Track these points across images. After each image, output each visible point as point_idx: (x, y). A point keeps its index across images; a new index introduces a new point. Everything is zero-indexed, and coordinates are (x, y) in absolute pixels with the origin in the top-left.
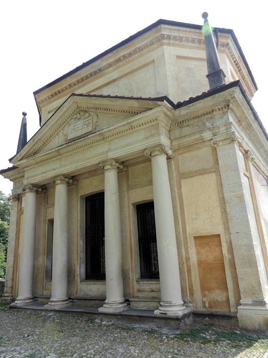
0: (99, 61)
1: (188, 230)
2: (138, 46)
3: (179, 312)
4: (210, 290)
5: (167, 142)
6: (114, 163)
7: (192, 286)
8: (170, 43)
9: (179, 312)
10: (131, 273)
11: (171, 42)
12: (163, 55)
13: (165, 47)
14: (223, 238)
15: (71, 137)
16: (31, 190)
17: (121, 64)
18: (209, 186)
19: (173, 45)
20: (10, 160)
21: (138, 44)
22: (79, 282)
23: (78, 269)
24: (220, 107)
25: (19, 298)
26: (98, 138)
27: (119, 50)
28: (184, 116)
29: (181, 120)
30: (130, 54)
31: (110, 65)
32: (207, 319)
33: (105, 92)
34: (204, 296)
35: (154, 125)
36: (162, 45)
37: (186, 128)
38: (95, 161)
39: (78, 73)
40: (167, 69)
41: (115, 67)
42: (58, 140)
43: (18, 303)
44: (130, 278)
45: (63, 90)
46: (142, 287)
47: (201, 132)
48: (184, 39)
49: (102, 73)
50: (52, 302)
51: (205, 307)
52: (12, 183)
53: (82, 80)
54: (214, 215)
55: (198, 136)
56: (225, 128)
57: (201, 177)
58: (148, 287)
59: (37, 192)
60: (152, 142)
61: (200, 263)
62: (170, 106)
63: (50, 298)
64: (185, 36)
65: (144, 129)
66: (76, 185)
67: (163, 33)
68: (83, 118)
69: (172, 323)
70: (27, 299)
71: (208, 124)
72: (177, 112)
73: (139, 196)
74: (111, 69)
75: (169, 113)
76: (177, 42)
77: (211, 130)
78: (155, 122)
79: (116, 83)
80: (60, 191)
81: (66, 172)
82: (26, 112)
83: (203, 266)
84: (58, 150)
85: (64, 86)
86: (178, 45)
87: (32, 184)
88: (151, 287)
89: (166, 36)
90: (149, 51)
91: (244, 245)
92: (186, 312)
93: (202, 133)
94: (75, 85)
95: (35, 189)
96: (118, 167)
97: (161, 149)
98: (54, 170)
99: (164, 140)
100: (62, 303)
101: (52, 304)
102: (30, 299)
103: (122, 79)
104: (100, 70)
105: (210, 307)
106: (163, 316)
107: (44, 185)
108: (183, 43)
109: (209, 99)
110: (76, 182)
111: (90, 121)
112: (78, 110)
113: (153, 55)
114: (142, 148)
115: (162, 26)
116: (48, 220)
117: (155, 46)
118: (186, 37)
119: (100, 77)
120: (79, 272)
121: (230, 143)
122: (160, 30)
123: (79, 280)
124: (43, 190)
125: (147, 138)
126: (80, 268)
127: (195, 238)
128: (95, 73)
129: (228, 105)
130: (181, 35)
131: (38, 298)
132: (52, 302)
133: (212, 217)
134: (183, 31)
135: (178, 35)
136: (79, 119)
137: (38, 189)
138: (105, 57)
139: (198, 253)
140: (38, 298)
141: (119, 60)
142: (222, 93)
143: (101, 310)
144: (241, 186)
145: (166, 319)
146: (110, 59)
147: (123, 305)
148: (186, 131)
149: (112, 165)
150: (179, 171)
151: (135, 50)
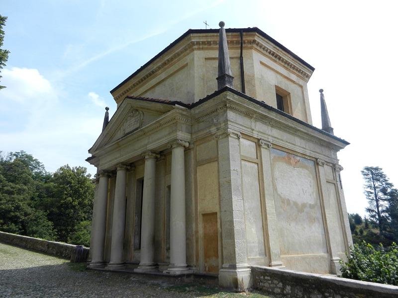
0: (151, 65)
1: (199, 208)
2: (176, 52)
3: (177, 272)
5: (186, 136)
6: (150, 154)
7: (198, 253)
8: (200, 48)
9: (177, 272)
10: (163, 243)
11: (201, 47)
12: (193, 59)
13: (195, 52)
15: (127, 131)
17: (166, 66)
18: (213, 172)
19: (202, 49)
20: (89, 151)
21: (177, 49)
23: (133, 240)
24: (221, 107)
25: (111, 263)
26: (141, 133)
27: (164, 55)
29: (197, 117)
30: (172, 58)
31: (159, 68)
33: (149, 95)
35: (174, 124)
36: (193, 50)
37: (201, 123)
38: (139, 152)
39: (138, 75)
41: (162, 69)
42: (120, 134)
43: (91, 265)
44: (161, 247)
45: (130, 89)
47: (210, 127)
48: (212, 43)
49: (155, 74)
50: (110, 264)
51: (205, 270)
53: (142, 80)
56: (224, 124)
57: (209, 165)
59: (127, 170)
60: (172, 137)
61: (205, 235)
62: (183, 107)
63: (140, 262)
64: (212, 40)
65: (169, 125)
66: (164, 159)
67: (193, 40)
68: (135, 115)
69: (172, 279)
70: (97, 263)
71: (215, 121)
72: (192, 111)
74: (160, 71)
75: (184, 113)
76: (206, 46)
77: (216, 126)
78: (175, 121)
79: (163, 83)
80: (120, 175)
81: (106, 168)
82: (108, 107)
84: (118, 143)
85: (130, 86)
86: (207, 49)
87: (104, 170)
89: (195, 43)
90: (185, 56)
91: (228, 221)
92: (186, 272)
94: (137, 84)
95: (106, 174)
96: (126, 168)
97: (175, 143)
98: (116, 158)
99: (182, 135)
100: (116, 266)
101: (110, 266)
102: (101, 263)
103: (168, 80)
104: (153, 72)
105: (209, 271)
106: (168, 274)
108: (212, 46)
109: (211, 100)
110: (133, 168)
112: (132, 109)
113: (188, 59)
114: (166, 141)
117: (188, 51)
118: (214, 41)
119: (154, 77)
120: (133, 243)
121: (226, 137)
123: (133, 249)
124: (132, 166)
125: (169, 134)
126: (134, 240)
127: (204, 215)
128: (150, 74)
129: (226, 105)
130: (209, 40)
131: (105, 262)
132: (110, 264)
134: (211, 36)
135: (205, 40)
136: (133, 116)
137: (127, 167)
138: (155, 61)
139: (205, 227)
140: (105, 262)
141: (165, 64)
142: (219, 96)
143: (136, 270)
144: (230, 173)
145: (169, 277)
146: (159, 63)
147: (150, 267)
148: (202, 125)
149: (149, 155)
150: (196, 160)
151: (175, 55)
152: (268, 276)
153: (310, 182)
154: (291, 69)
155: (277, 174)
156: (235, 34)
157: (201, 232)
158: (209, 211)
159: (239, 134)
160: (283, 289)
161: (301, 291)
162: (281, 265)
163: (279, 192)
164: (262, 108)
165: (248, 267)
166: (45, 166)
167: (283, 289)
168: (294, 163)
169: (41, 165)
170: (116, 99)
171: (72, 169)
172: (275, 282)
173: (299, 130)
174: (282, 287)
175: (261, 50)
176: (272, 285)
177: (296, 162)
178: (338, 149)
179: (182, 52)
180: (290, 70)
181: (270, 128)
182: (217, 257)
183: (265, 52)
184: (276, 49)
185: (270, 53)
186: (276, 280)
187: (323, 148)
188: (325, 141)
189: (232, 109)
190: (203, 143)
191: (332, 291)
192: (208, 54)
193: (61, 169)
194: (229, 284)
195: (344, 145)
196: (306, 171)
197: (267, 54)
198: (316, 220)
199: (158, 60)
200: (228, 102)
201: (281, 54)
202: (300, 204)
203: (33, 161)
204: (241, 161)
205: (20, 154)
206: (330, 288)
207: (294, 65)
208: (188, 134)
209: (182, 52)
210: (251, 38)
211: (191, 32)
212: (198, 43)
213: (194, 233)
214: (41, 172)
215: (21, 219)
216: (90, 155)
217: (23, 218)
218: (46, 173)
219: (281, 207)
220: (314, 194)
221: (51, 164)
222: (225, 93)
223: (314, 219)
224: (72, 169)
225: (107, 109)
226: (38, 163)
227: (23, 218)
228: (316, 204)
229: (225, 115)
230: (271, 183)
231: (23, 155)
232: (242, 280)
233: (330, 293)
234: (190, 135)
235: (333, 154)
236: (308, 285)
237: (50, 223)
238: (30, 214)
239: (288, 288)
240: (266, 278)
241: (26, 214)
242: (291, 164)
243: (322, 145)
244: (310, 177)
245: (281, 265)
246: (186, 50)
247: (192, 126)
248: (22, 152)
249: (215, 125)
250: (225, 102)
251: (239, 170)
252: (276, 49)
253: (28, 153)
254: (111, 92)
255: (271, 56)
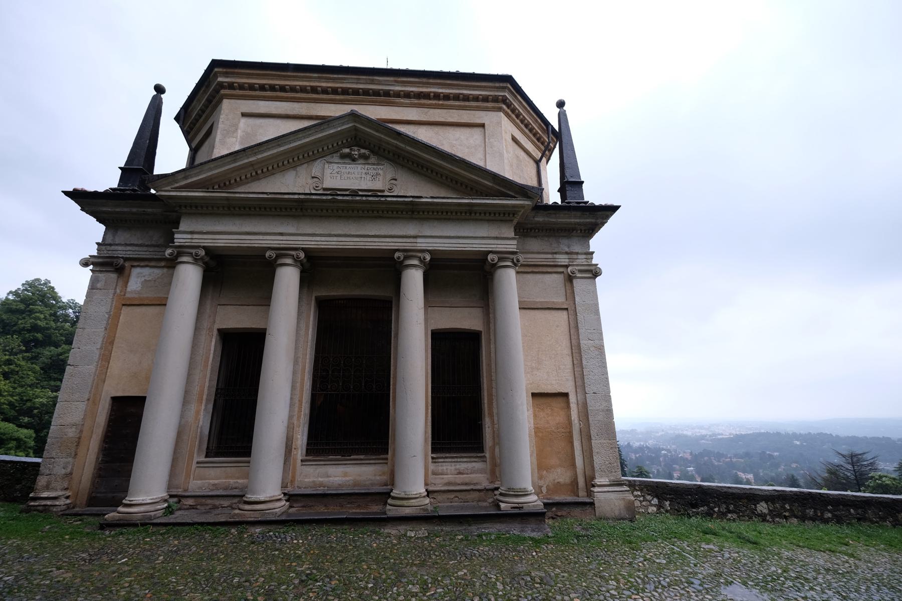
4: (548, 469)
14: (572, 398)
16: (196, 260)
18: (557, 326)
22: (299, 462)
28: (538, 222)
32: (554, 509)
46: (440, 468)
52: (102, 228)
54: (562, 367)
58: (453, 468)
73: (238, 318)
83: (540, 435)
88: (458, 467)
106: (516, 511)
116: (219, 330)
127: (534, 395)
133: (560, 369)
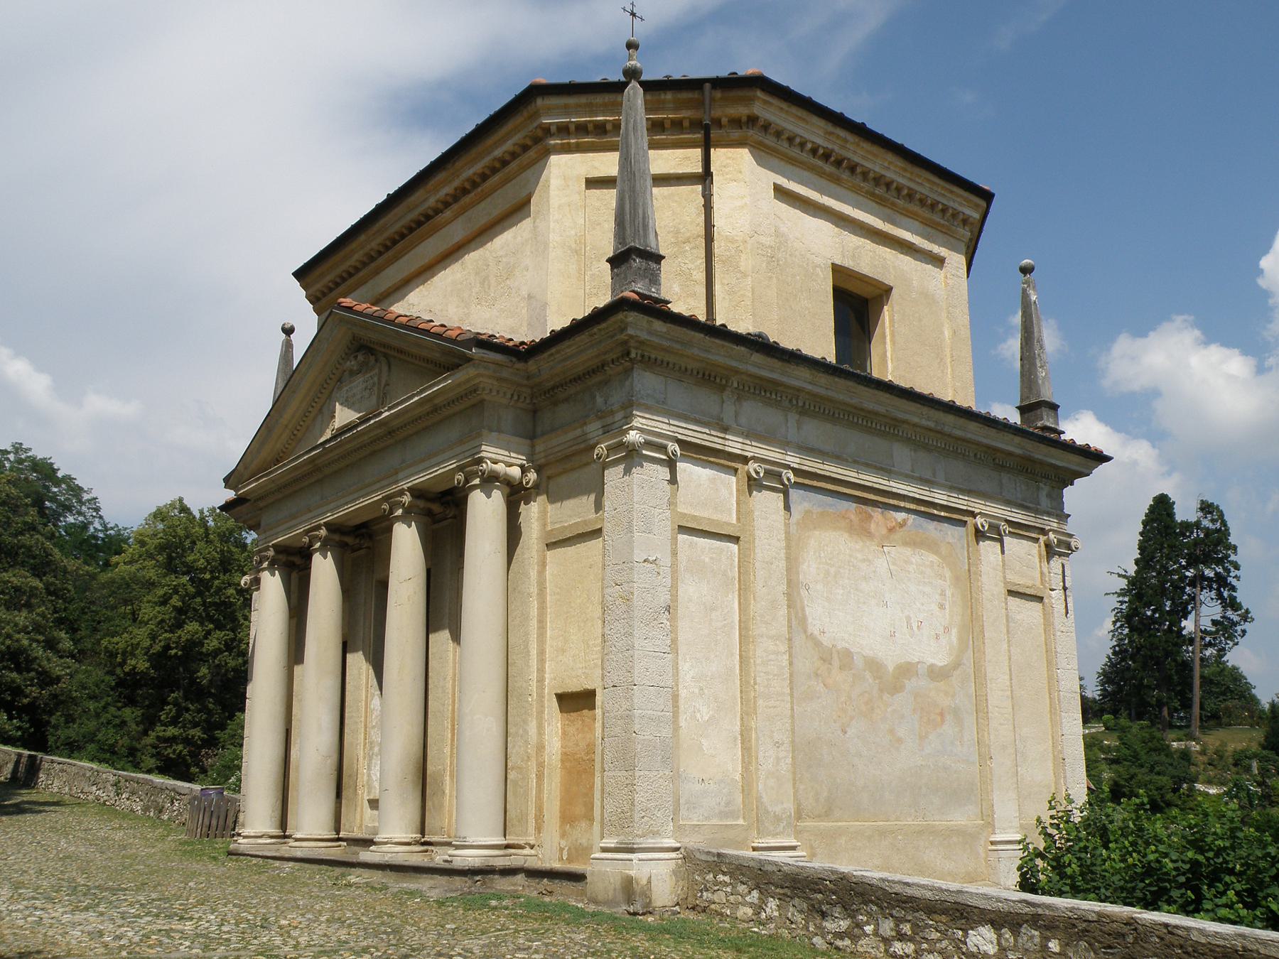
13: (554, 159)
25: (246, 831)
34: (563, 835)
40: (552, 225)
43: (242, 844)
55: (578, 432)
61: (566, 757)
66: (368, 548)
72: (532, 365)
74: (448, 214)
82: (290, 322)
93: (585, 424)
105: (570, 860)
106: (447, 866)
107: (364, 525)
111: (376, 379)
115: (540, 102)
122: (536, 115)
129: (628, 354)
138: (432, 183)
152: (724, 874)
153: (943, 594)
154: (900, 202)
155: (810, 568)
156: (685, 95)
157: (554, 746)
158: (574, 686)
159: (673, 447)
160: (758, 908)
161: (801, 912)
162: (793, 848)
163: (814, 628)
164: (757, 358)
165: (677, 849)
166: (102, 503)
167: (758, 908)
168: (884, 531)
169: (86, 497)
170: (314, 299)
171: (198, 516)
172: (742, 888)
173: (905, 422)
174: (756, 901)
175: (783, 146)
176: (732, 898)
177: (891, 530)
178: (1068, 478)
179: (514, 155)
180: (894, 204)
181: (793, 417)
182: (592, 820)
183: (795, 152)
184: (838, 137)
185: (814, 151)
186: (743, 883)
187: (1005, 477)
188: (1010, 454)
189: (650, 363)
190: (565, 472)
191: (875, 908)
192: (596, 164)
193: (159, 515)
194: (611, 893)
195: (1090, 463)
196: (933, 558)
197: (805, 157)
198: (948, 717)
199: (441, 176)
200: (632, 343)
201: (858, 152)
202: (891, 669)
203: (58, 482)
204: (674, 541)
205: (12, 457)
206: (872, 902)
207: (912, 185)
208: (517, 439)
209: (514, 155)
210: (741, 111)
211: (534, 92)
212: (564, 130)
213: (532, 751)
214: (85, 526)
215: (26, 697)
216: (230, 495)
217: (34, 691)
218: (106, 529)
219: (817, 675)
220: (954, 631)
221: (125, 498)
222: (620, 316)
223: (942, 714)
224: (198, 516)
225: (288, 331)
226: (77, 491)
227: (34, 691)
228: (957, 665)
229: (627, 383)
230: (783, 601)
231: (20, 461)
232: (649, 882)
233: (869, 914)
234: (528, 441)
235: (1049, 496)
236: (820, 896)
237: (128, 713)
238: (58, 679)
239: (772, 904)
240: (721, 878)
241: (46, 679)
242: (869, 535)
243: (1001, 467)
244: (942, 577)
245: (793, 848)
246: (525, 148)
247: (535, 412)
248: (18, 448)
249: (601, 415)
250: (626, 342)
251: (666, 560)
252: (838, 137)
253: (39, 453)
254: (300, 274)
255: (820, 163)
